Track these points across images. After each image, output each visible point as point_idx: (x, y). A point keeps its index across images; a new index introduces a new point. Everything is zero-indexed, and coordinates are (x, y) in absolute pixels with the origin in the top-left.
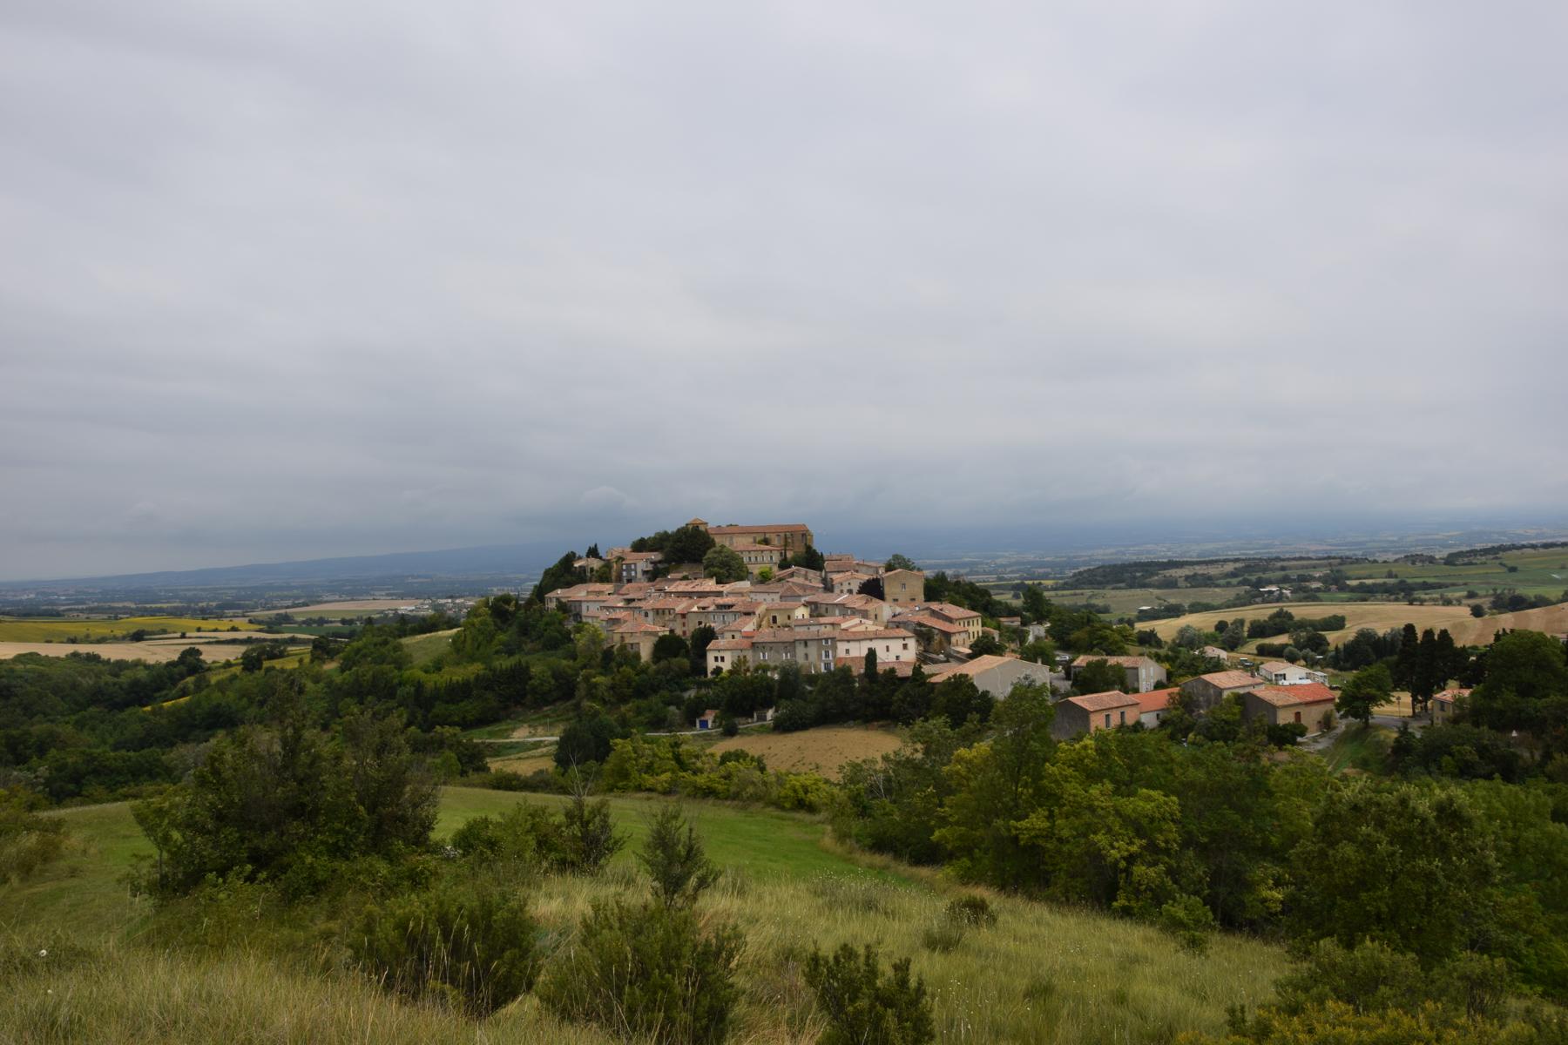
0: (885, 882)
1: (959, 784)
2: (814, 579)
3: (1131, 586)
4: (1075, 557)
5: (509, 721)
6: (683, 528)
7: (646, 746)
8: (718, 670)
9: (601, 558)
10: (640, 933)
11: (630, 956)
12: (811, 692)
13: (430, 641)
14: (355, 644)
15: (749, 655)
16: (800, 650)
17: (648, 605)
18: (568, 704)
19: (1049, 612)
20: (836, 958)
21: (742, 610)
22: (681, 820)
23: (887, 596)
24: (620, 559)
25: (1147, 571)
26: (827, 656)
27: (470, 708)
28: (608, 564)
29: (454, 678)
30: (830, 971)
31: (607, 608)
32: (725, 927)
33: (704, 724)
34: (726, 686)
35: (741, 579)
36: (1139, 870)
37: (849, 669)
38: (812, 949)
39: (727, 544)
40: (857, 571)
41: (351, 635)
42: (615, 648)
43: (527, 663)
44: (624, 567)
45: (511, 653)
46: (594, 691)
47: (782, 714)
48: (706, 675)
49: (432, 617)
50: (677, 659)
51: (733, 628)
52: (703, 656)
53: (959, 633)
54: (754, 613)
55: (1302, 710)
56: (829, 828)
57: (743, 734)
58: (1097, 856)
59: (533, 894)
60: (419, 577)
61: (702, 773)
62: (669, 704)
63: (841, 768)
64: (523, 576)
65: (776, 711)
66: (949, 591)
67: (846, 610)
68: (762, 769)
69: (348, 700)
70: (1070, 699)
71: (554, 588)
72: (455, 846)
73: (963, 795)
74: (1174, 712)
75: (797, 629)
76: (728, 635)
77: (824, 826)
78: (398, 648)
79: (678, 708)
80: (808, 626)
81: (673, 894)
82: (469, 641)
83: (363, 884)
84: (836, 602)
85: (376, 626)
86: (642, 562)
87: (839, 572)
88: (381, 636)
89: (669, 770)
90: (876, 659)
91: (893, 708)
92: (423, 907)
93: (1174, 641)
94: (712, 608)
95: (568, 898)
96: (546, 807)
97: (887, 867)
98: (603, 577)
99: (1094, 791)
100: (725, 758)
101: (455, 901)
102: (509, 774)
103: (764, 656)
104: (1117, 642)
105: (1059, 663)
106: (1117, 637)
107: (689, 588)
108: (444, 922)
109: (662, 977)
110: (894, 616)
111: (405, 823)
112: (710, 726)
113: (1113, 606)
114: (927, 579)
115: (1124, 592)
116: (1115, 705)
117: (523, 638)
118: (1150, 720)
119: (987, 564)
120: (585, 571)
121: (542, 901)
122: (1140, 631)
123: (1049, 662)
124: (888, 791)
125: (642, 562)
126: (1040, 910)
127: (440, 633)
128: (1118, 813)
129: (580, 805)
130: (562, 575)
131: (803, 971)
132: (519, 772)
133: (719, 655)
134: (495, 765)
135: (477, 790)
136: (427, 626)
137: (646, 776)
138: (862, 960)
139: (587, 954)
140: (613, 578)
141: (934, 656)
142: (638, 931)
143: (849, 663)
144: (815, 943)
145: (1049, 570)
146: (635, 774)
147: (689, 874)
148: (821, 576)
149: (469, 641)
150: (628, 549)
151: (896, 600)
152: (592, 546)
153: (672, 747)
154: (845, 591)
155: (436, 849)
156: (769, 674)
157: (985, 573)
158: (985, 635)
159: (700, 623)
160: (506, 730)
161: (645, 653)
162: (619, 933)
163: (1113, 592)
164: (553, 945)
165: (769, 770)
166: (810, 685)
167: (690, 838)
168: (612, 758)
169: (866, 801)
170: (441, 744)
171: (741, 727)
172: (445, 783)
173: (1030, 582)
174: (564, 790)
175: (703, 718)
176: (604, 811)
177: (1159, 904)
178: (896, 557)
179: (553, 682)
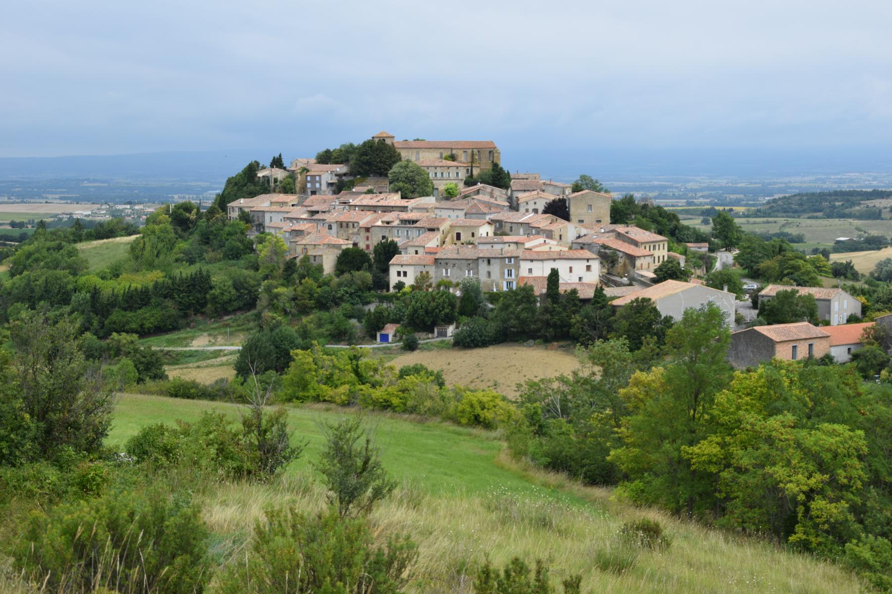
0: (558, 500)
1: (636, 407)
2: (500, 196)
3: (829, 216)
4: (770, 184)
5: (188, 329)
6: (369, 141)
7: (325, 357)
8: (400, 286)
9: (285, 168)
10: (313, 541)
11: (302, 563)
12: (492, 310)
13: (109, 243)
14: (26, 248)
15: (432, 271)
16: (483, 268)
17: (330, 218)
18: (249, 314)
19: (739, 239)
20: (507, 573)
21: (427, 225)
22: (359, 431)
23: (572, 217)
24: (305, 170)
25: (848, 201)
26: (510, 274)
27: (149, 316)
28: (292, 176)
29: (134, 285)
30: (500, 584)
31: (291, 219)
32: (398, 537)
33: (385, 338)
34: (408, 301)
36: (818, 504)
37: (531, 289)
38: (483, 562)
39: (413, 159)
40: (543, 191)
41: (22, 238)
42: (298, 260)
43: (208, 271)
44: (309, 178)
45: (191, 262)
46: (275, 301)
47: (462, 332)
48: (388, 290)
49: (109, 223)
50: (360, 272)
51: (416, 244)
52: (386, 270)
53: (644, 256)
54: (438, 229)
55: (513, 225)
56: (505, 445)
57: (422, 349)
58: (774, 489)
59: (208, 501)
60: (95, 181)
61: (381, 386)
62: (351, 317)
63: (519, 386)
64: (204, 184)
65: (457, 328)
66: (636, 214)
67: (530, 229)
68: (441, 385)
69: (19, 305)
70: (756, 328)
71: (236, 197)
72: (129, 452)
73: (640, 417)
74: (867, 347)
75: (481, 247)
76: (412, 251)
77: (500, 443)
78: (71, 254)
79: (360, 321)
80: (492, 244)
81: (348, 504)
82: (148, 248)
83: (30, 491)
84: (520, 221)
85: (49, 230)
86: (328, 174)
87: (525, 191)
88: (54, 240)
89: (348, 383)
90: (558, 280)
91: (572, 330)
92: (93, 512)
93: (872, 274)
95: (244, 505)
96: (224, 416)
97: (560, 487)
98: (287, 188)
99: (774, 422)
100: (404, 373)
101: (126, 506)
102: (187, 382)
103: (447, 273)
104: (808, 273)
105: (746, 292)
106: (810, 267)
107: (373, 202)
108: (113, 526)
109: (333, 585)
110: (579, 237)
111: (78, 429)
112: (390, 340)
113: (807, 235)
114: (614, 202)
115: (820, 221)
116: (804, 337)
117: (205, 247)
118: (840, 354)
119: (676, 188)
120: (268, 181)
121: (217, 508)
122: (835, 263)
123: (736, 289)
124: (565, 411)
125: (328, 174)
126: (716, 539)
127: (118, 239)
128: (799, 445)
129: (258, 415)
130: (245, 185)
131: (474, 584)
132: (198, 381)
133: (402, 270)
134: (173, 373)
135: (154, 397)
136: (104, 232)
137: (324, 387)
138: (532, 576)
139: (260, 560)
140: (297, 189)
141: (617, 279)
142: (312, 539)
143: (531, 283)
144: (487, 555)
145: (742, 196)
146: (314, 384)
147: (367, 485)
148: (506, 194)
149: (148, 248)
151: (581, 221)
152: (277, 156)
153: (351, 360)
154: (530, 210)
155: (109, 456)
156: (451, 290)
157: (674, 197)
158: (671, 260)
159: (384, 237)
160: (185, 338)
161: (328, 265)
162: (291, 540)
163: (809, 222)
164: (226, 553)
165: (448, 386)
166: (492, 303)
167: (367, 449)
168: (293, 369)
169: (542, 419)
170: (118, 352)
171: (421, 342)
172: (120, 390)
173: (721, 208)
174: (242, 399)
175: (383, 332)
176: (282, 420)
177: (843, 543)
178: (583, 178)
179: (233, 292)
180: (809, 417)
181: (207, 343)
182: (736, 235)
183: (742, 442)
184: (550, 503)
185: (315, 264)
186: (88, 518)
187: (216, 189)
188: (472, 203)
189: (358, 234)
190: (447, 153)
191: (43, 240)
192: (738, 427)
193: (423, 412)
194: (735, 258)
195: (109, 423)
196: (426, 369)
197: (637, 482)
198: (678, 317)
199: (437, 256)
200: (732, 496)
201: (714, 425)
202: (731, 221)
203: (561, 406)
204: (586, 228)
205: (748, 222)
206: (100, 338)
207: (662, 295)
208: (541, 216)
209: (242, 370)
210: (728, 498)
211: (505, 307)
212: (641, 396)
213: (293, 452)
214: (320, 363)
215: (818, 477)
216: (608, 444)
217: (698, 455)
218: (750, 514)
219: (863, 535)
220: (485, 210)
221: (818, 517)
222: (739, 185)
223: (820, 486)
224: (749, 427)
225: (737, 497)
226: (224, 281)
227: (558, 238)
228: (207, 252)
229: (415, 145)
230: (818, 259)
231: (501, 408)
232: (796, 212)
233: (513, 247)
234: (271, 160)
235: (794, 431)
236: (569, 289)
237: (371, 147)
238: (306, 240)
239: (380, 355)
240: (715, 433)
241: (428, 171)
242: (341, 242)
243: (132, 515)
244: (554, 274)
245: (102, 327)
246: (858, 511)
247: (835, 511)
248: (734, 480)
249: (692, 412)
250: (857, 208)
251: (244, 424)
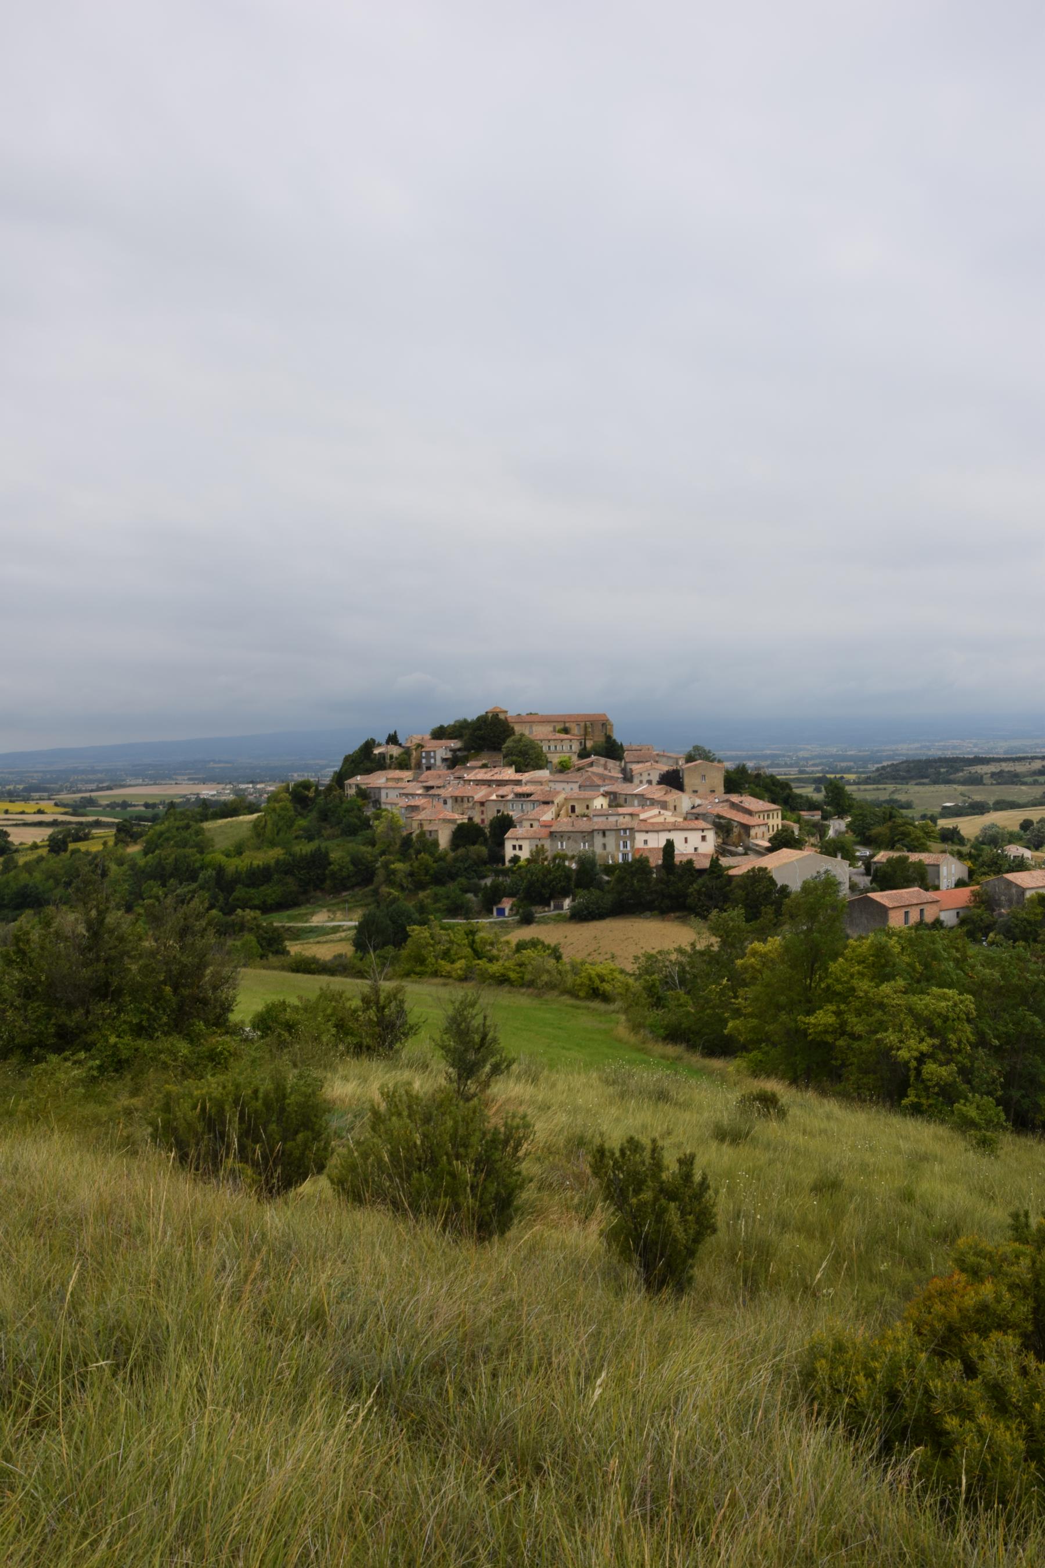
1: (754, 978)
2: (613, 768)
3: (935, 782)
4: (878, 751)
7: (442, 932)
8: (515, 859)
9: (400, 745)
12: (608, 882)
14: (158, 828)
16: (598, 840)
18: (367, 889)
19: (851, 806)
20: (622, 1152)
21: (542, 799)
23: (686, 788)
24: (420, 746)
26: (625, 846)
27: (271, 892)
28: (407, 752)
29: (255, 863)
30: (616, 1162)
31: (406, 795)
33: (501, 912)
34: (524, 875)
35: (541, 768)
36: (930, 1068)
37: (647, 860)
38: (597, 1141)
39: (527, 733)
40: (657, 762)
41: (154, 819)
42: (414, 835)
43: (326, 848)
44: (424, 754)
45: (310, 839)
47: (579, 903)
48: (504, 863)
49: (233, 802)
50: (476, 847)
52: (501, 845)
53: (759, 825)
54: (553, 802)
56: (623, 1018)
57: (539, 923)
58: (885, 1053)
59: (329, 1075)
60: (220, 762)
61: (497, 960)
62: (467, 891)
63: (636, 958)
65: (573, 900)
67: (645, 801)
68: (558, 958)
69: (151, 882)
70: (869, 895)
75: (596, 819)
76: (527, 824)
79: (476, 895)
80: (607, 815)
83: (164, 1063)
84: (635, 792)
85: (179, 810)
86: (442, 750)
91: (689, 901)
93: (977, 838)
94: (511, 797)
95: (364, 1080)
96: (343, 992)
97: (679, 1058)
98: (403, 764)
99: (886, 988)
100: (521, 947)
102: (307, 958)
105: (859, 858)
110: (693, 807)
112: (507, 914)
114: (727, 772)
115: (927, 787)
116: (915, 902)
118: (949, 918)
119: (789, 756)
120: (384, 758)
122: (942, 828)
123: (850, 857)
124: (683, 982)
125: (442, 750)
126: (832, 1106)
127: (241, 818)
128: (911, 1010)
129: (376, 991)
130: (362, 762)
132: (318, 956)
133: (517, 843)
135: (276, 973)
136: (228, 810)
137: (442, 962)
138: (647, 1154)
140: (413, 765)
141: (733, 848)
142: (427, 1119)
143: (646, 854)
145: (852, 764)
146: (431, 960)
147: (484, 1061)
150: (428, 736)
151: (695, 792)
152: (392, 732)
154: (644, 781)
155: (234, 1030)
157: (786, 765)
158: (785, 829)
159: (498, 811)
160: (306, 914)
161: (444, 839)
162: (408, 1121)
163: (917, 788)
165: (565, 959)
166: (607, 875)
167: (484, 1025)
169: (661, 992)
172: (245, 966)
173: (832, 776)
174: (361, 974)
175: (500, 906)
176: (399, 996)
178: (696, 748)
179: (351, 868)
180: (918, 981)
181: (326, 918)
182: (847, 803)
183: (856, 1010)
184: (668, 1076)
185: (431, 839)
186: (216, 1094)
187: (334, 766)
188: (586, 775)
189: (473, 808)
190: (559, 727)
191: (172, 819)
192: (852, 996)
193: (540, 986)
194: (848, 826)
195: (234, 999)
196: (543, 943)
197: (755, 1052)
198: (795, 886)
199: (552, 829)
200: (848, 1063)
201: (830, 995)
202: (843, 789)
203: (679, 978)
204: (700, 798)
205: (859, 790)
206: (225, 914)
207: (777, 864)
208: (655, 787)
209: (359, 945)
210: (843, 1065)
211: (620, 880)
212: (758, 967)
213: (411, 1028)
214: (437, 939)
215: (930, 1041)
216: (726, 1015)
217: (814, 1025)
218: (865, 1080)
219: (970, 1095)
220: (599, 782)
221: (929, 1080)
222: (849, 753)
223: (931, 1050)
224: (862, 994)
225: (851, 1064)
226: (343, 857)
227: (672, 808)
228: (325, 829)
229: (528, 719)
230: (927, 825)
231: (619, 981)
232: (903, 778)
233: (628, 818)
234: (386, 737)
235: (905, 996)
236: (685, 859)
237: (485, 722)
238: (422, 816)
239: (497, 929)
240: (831, 1002)
241: (541, 744)
242: (457, 816)
243: (256, 1092)
244: (670, 845)
245: (226, 904)
246: (964, 1072)
247: (945, 1074)
248: (849, 1047)
249: (808, 981)
250: (961, 774)
251: (363, 1000)
